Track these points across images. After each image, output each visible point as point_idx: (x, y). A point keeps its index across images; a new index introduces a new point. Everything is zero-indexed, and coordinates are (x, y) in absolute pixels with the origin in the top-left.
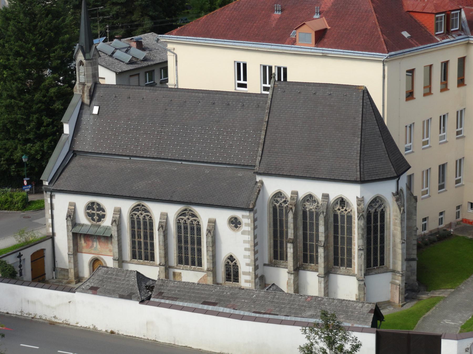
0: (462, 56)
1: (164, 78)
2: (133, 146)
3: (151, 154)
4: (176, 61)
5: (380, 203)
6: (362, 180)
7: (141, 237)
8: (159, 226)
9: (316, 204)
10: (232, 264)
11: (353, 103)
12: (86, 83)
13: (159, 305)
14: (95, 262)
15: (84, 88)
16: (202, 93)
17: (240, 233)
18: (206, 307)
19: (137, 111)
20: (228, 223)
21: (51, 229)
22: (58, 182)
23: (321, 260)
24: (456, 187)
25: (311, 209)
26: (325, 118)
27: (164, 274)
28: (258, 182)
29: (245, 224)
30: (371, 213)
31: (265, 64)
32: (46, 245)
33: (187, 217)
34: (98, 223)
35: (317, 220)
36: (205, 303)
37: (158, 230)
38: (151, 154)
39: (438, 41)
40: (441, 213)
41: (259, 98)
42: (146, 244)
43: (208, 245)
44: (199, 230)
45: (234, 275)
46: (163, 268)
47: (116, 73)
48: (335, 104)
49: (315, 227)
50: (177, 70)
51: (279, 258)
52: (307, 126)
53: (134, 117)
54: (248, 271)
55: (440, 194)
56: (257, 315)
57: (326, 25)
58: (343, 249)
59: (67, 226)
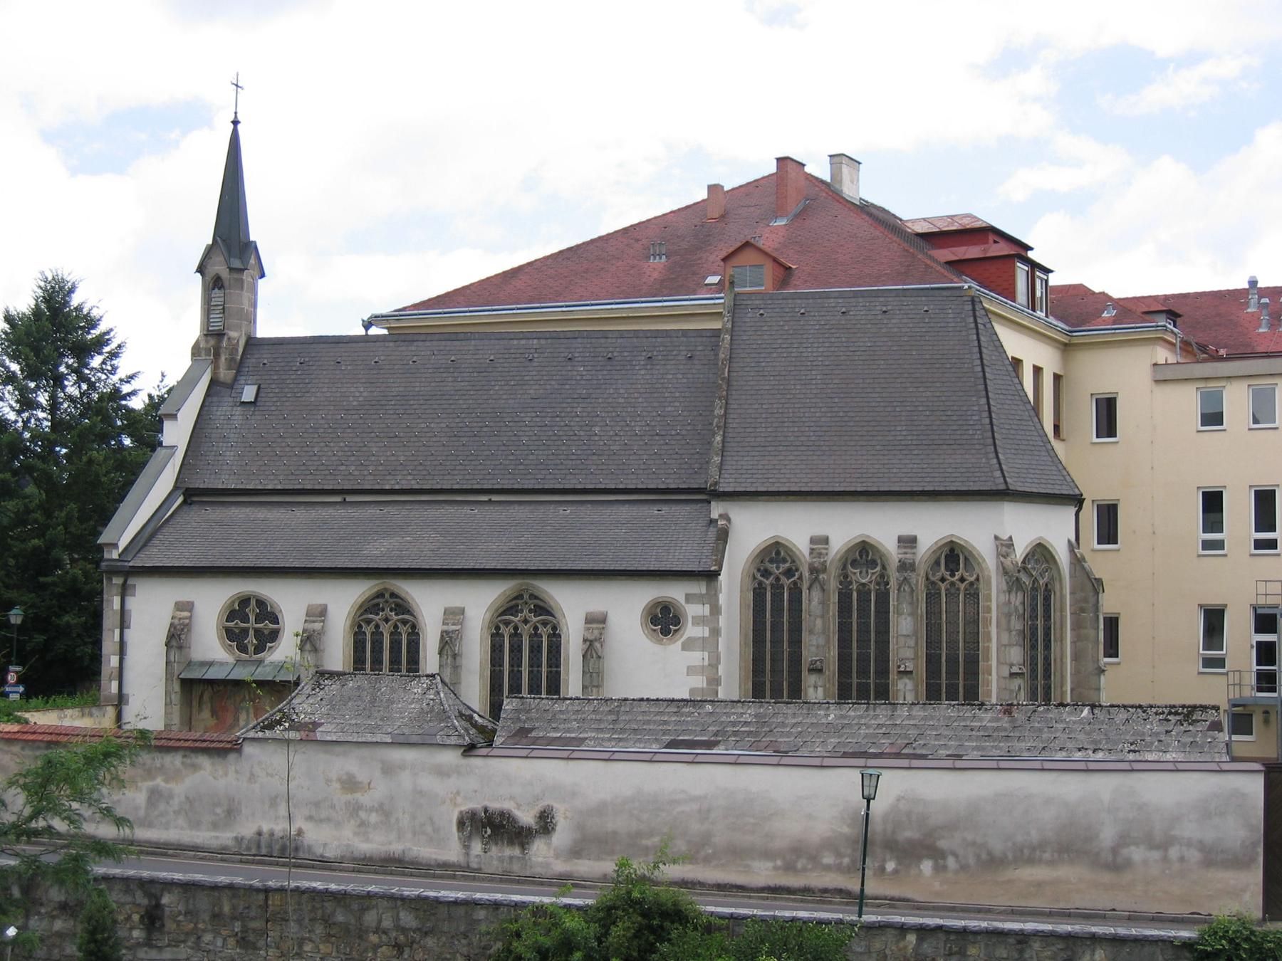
15: (220, 341)
19: (362, 390)
25: (864, 585)
38: (403, 482)
41: (693, 339)
43: (586, 684)
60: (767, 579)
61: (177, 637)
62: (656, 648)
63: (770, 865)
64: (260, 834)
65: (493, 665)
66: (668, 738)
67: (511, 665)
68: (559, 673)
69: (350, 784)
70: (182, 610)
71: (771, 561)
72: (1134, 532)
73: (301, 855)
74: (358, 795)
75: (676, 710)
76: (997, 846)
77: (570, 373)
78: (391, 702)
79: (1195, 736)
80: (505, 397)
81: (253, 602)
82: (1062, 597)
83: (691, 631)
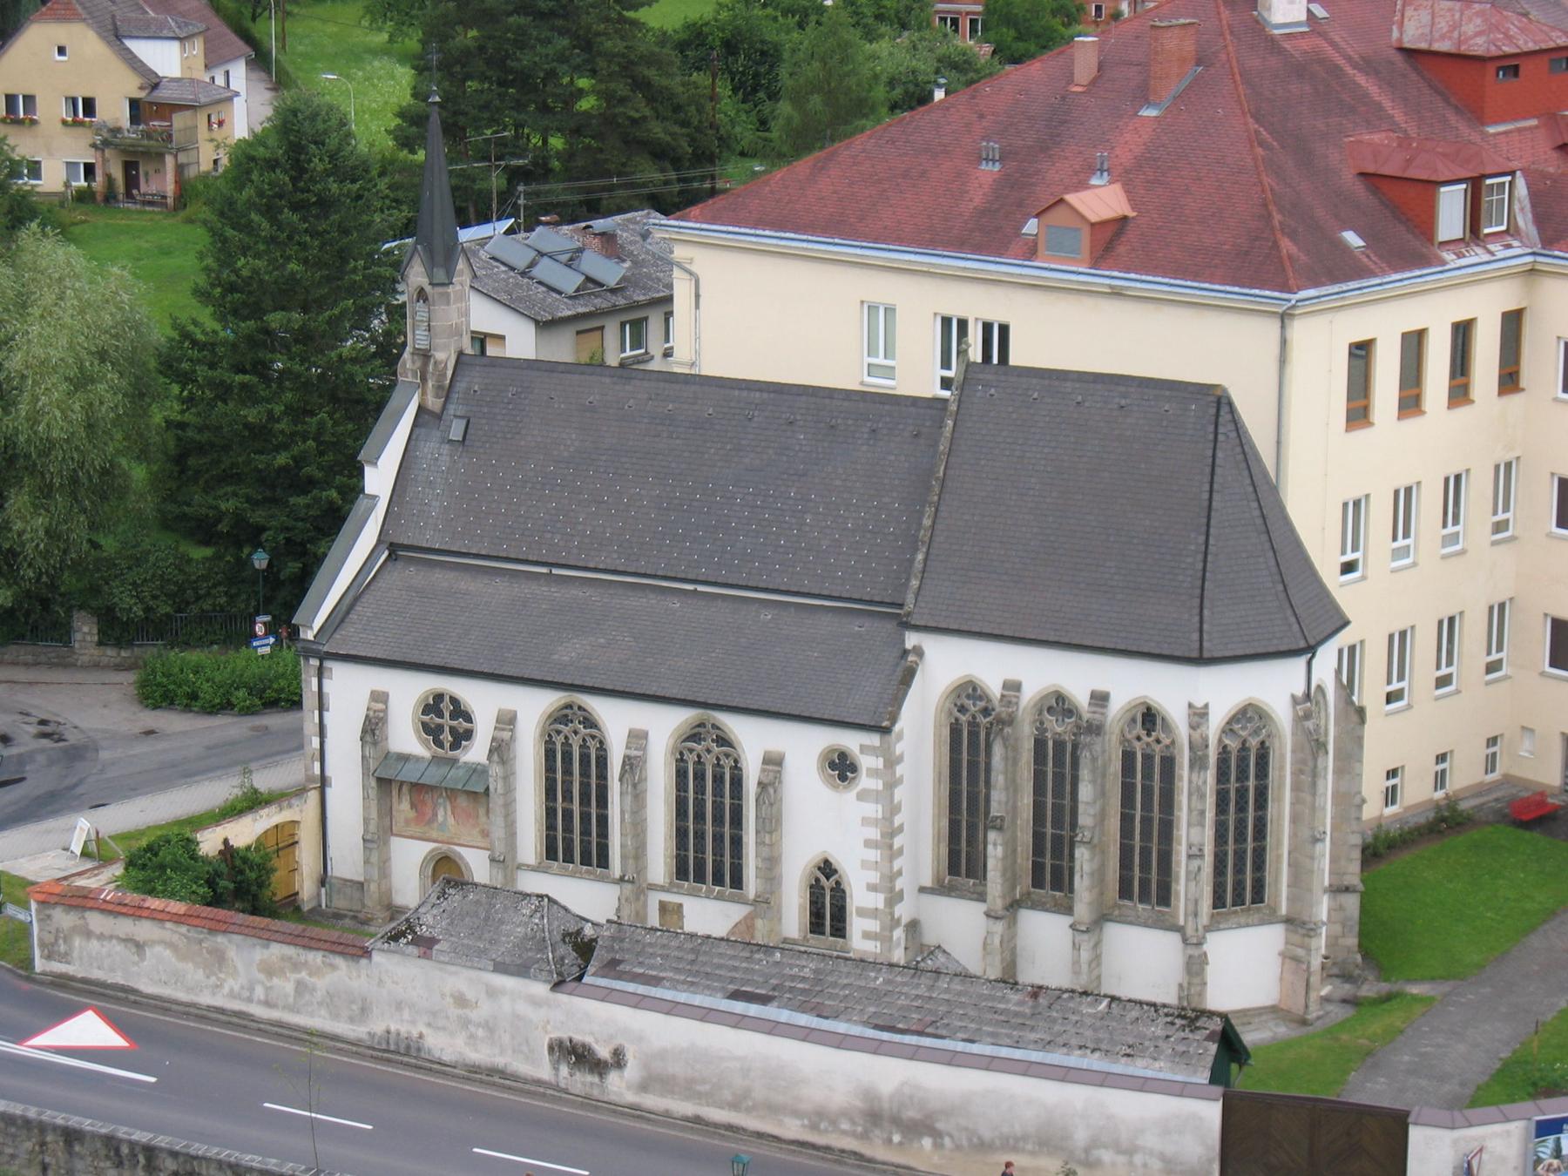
1: (631, 350)
2: (559, 536)
3: (608, 561)
4: (697, 296)
10: (827, 884)
11: (1190, 432)
13: (607, 996)
15: (425, 364)
16: (761, 390)
17: (851, 795)
18: (739, 1007)
21: (317, 765)
24: (1488, 683)
29: (868, 769)
31: (948, 312)
36: (736, 995)
37: (621, 780)
38: (608, 561)
39: (1444, 263)
40: (1441, 758)
41: (922, 411)
44: (737, 782)
47: (537, 322)
49: (1068, 788)
53: (566, 454)
54: (871, 905)
56: (885, 1036)
61: (373, 728)
63: (798, 1122)
64: (388, 1032)
65: (678, 790)
66: (732, 987)
67: (696, 793)
69: (461, 1001)
70: (376, 701)
71: (968, 697)
73: (423, 1055)
74: (467, 1011)
75: (748, 955)
76: (987, 1135)
78: (501, 922)
79: (1189, 1046)
80: (719, 464)
81: (447, 699)
82: (1283, 756)
83: (865, 782)
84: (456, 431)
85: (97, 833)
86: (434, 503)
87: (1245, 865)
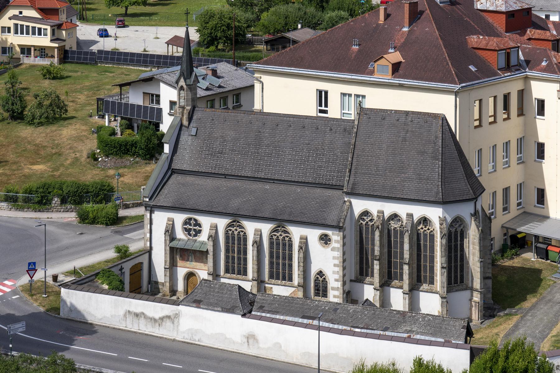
0: (521, 88)
3: (245, 173)
4: (263, 88)
5: (460, 223)
6: (444, 201)
7: (235, 252)
8: (253, 241)
9: (401, 222)
10: (321, 279)
12: (186, 107)
13: (261, 318)
14: (190, 276)
15: (183, 110)
18: (305, 321)
19: (232, 133)
20: (319, 239)
22: (157, 198)
23: (406, 277)
25: (396, 228)
26: (408, 143)
27: (257, 288)
28: (346, 201)
29: (335, 240)
30: (458, 232)
32: (144, 259)
33: (280, 233)
34: (194, 238)
35: (402, 237)
36: (304, 317)
37: (253, 246)
38: (245, 173)
42: (239, 259)
44: (291, 246)
45: (323, 290)
46: (255, 282)
48: (417, 130)
50: (263, 96)
51: (364, 275)
52: (391, 149)
53: (230, 139)
55: (504, 216)
57: (401, 59)
58: (425, 266)
59: (165, 240)
60: (364, 222)
62: (322, 249)
68: (292, 254)
72: (550, 157)
77: (303, 133)
84: (193, 133)
85: (75, 268)
86: (186, 155)
87: (457, 270)
